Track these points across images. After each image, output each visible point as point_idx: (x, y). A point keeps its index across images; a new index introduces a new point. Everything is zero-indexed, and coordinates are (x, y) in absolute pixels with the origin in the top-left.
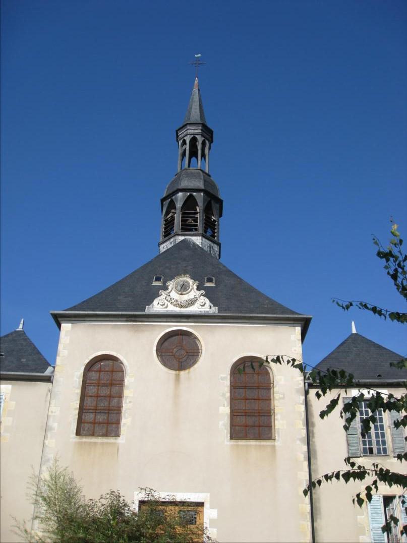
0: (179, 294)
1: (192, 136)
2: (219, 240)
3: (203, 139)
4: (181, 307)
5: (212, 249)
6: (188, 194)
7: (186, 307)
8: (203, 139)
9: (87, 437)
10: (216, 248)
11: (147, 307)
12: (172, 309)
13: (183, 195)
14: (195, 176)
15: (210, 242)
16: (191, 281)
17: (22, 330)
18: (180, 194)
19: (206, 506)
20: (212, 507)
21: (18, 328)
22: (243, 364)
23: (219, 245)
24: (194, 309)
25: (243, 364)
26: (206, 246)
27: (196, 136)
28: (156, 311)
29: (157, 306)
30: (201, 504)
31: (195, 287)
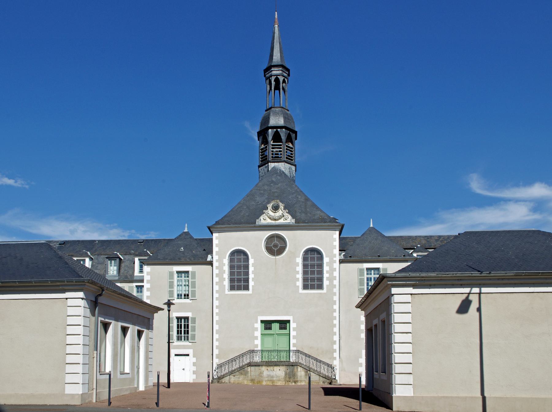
0: (273, 212)
1: (276, 77)
2: (295, 162)
3: (283, 78)
4: (275, 220)
5: (291, 170)
6: (275, 130)
7: (278, 220)
8: (283, 78)
9: (145, 346)
10: (293, 168)
11: (257, 220)
12: (269, 221)
13: (272, 131)
14: (278, 114)
15: (289, 165)
16: (281, 204)
17: (187, 231)
18: (270, 130)
19: (291, 322)
20: (294, 322)
21: (185, 230)
22: (472, 292)
23: (295, 166)
24: (281, 221)
25: (467, 295)
26: (288, 169)
27: (278, 77)
28: (262, 223)
29: (264, 220)
30: (288, 321)
31: (282, 208)
